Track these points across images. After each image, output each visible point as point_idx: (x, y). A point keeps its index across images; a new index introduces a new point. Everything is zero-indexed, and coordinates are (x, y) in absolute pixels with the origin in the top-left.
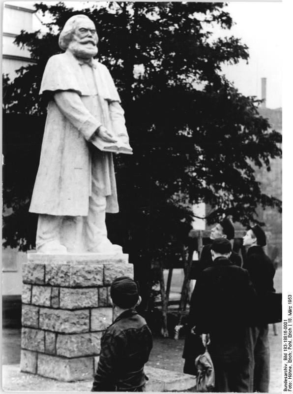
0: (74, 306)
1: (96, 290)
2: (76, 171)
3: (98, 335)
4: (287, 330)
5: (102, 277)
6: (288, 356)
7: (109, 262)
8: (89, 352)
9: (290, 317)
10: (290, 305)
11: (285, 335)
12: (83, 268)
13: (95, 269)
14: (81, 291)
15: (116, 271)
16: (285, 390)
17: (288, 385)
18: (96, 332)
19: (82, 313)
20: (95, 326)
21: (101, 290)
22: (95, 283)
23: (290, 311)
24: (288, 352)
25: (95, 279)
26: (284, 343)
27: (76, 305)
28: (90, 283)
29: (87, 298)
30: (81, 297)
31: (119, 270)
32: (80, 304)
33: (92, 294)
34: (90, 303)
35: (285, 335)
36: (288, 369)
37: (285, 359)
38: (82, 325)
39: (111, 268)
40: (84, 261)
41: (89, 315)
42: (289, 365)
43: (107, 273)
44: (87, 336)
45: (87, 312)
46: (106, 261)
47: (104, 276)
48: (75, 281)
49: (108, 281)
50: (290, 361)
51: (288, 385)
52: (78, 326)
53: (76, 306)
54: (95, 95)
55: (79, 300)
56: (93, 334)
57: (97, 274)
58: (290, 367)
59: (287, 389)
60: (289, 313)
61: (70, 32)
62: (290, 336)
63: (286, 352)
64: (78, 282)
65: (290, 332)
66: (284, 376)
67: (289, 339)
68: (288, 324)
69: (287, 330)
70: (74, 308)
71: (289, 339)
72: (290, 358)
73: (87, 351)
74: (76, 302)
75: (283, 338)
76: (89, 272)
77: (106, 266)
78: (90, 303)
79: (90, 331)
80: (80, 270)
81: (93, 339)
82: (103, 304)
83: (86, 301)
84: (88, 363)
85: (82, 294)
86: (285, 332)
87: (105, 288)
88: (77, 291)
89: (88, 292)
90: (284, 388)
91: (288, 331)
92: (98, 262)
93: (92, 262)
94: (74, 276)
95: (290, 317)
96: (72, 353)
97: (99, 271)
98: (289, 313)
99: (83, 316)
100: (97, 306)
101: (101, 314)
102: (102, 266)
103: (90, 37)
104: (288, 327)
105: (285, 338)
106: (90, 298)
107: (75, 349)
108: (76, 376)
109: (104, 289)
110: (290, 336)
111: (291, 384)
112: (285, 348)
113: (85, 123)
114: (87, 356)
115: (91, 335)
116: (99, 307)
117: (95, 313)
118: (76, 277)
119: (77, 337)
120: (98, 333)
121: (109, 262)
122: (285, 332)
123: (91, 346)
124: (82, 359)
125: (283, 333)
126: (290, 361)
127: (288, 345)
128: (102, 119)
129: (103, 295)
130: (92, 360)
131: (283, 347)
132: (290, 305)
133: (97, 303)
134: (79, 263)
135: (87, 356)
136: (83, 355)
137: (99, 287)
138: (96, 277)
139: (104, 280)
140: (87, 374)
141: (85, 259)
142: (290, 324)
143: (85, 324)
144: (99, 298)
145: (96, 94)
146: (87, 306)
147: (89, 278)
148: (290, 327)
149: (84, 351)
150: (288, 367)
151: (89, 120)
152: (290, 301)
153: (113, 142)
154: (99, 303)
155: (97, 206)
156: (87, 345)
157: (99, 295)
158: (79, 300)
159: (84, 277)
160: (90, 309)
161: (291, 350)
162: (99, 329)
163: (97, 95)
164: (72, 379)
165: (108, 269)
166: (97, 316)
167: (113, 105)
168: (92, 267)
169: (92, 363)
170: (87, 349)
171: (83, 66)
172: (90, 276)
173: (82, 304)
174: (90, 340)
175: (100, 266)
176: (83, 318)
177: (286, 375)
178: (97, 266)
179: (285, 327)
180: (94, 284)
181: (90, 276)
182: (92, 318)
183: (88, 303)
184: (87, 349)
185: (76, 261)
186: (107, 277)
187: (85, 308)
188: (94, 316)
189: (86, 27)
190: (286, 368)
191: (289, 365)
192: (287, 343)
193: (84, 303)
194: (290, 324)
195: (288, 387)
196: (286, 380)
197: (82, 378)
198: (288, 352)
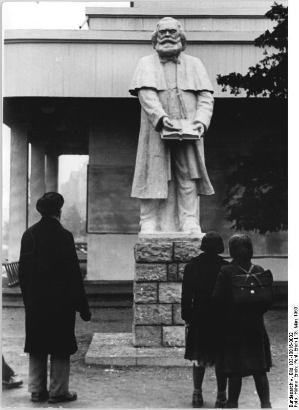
0: (140, 279)
1: (164, 266)
2: (155, 158)
3: (166, 307)
4: (293, 343)
5: (171, 254)
6: (294, 371)
7: (182, 240)
8: (156, 322)
9: (295, 330)
10: (296, 317)
11: (291, 349)
12: (149, 245)
13: (163, 246)
14: (147, 265)
15: (188, 249)
16: (291, 406)
17: (294, 400)
18: (165, 304)
19: (149, 285)
20: (163, 297)
21: (170, 266)
22: (162, 259)
23: (296, 324)
24: (294, 366)
25: (162, 256)
26: (289, 357)
27: (142, 278)
28: (156, 259)
29: (154, 272)
30: (147, 271)
31: (191, 248)
32: (146, 278)
33: (160, 269)
34: (157, 276)
35: (291, 349)
36: (294, 384)
37: (291, 374)
38: (148, 296)
39: (182, 246)
40: (154, 239)
41: (156, 287)
42: (295, 380)
43: (176, 251)
44: (154, 307)
45: (154, 285)
46: (175, 239)
47: (173, 252)
48: (140, 257)
49: (177, 258)
50: (296, 376)
51: (294, 400)
52: (144, 297)
53: (142, 279)
54: (174, 89)
55: (145, 273)
56: (160, 306)
57: (165, 251)
58: (296, 382)
59: (293, 405)
60: (295, 326)
61: (154, 35)
62: (296, 350)
63: (291, 367)
64: (144, 257)
65: (296, 346)
66: (289, 392)
67: (295, 353)
68: (294, 337)
69: (293, 343)
70: (140, 281)
71: (295, 353)
72: (296, 372)
73: (154, 321)
74: (143, 276)
75: (289, 352)
76: (156, 249)
77: (176, 244)
78: (157, 276)
79: (158, 302)
80: (146, 247)
81: (160, 310)
82: (171, 278)
83: (153, 275)
84: (155, 332)
85: (149, 268)
86: (290, 345)
87: (176, 265)
88: (143, 266)
89: (156, 267)
90: (289, 403)
91: (294, 345)
92: (169, 240)
93: (162, 240)
94: (139, 252)
95: (295, 330)
96: (138, 321)
97: (167, 249)
98: (295, 326)
99: (150, 288)
100: (166, 280)
101: (168, 288)
102: (171, 244)
103: (168, 37)
104: (294, 340)
105: (291, 352)
106: (158, 273)
107: (141, 317)
108: (141, 342)
109: (174, 266)
110: (296, 350)
111: (296, 399)
112: (290, 362)
113: (152, 115)
114: (154, 325)
115: (158, 307)
116: (168, 281)
117: (162, 286)
118: (141, 253)
119: (143, 307)
120: (167, 305)
121: (182, 240)
122: (290, 345)
123: (159, 317)
124: (149, 327)
125: (289, 347)
126: (296, 376)
127: (294, 359)
128: (181, 110)
129: (172, 271)
130: (160, 329)
131: (289, 361)
132: (296, 317)
133: (166, 278)
134: (148, 240)
135: (154, 325)
136: (151, 323)
137: (167, 263)
138: (163, 253)
139: (173, 257)
140: (153, 341)
141: (155, 237)
142: (296, 337)
143: (152, 295)
144: (168, 273)
145: (175, 87)
146: (154, 279)
147: (155, 254)
148: (296, 340)
149: (150, 320)
150: (294, 382)
151: (155, 113)
152: (296, 313)
153: (177, 130)
154: (167, 278)
155: (184, 189)
156: (154, 315)
157: (168, 270)
158: (145, 273)
159: (149, 253)
160: (158, 282)
161: (298, 364)
162: (168, 302)
163: (177, 88)
164: (138, 344)
165: (179, 247)
166: (165, 289)
167: (200, 95)
168: (159, 245)
169: (160, 332)
170: (154, 318)
171: (166, 64)
172: (156, 253)
173: (149, 278)
174: (157, 311)
175: (169, 244)
176: (149, 290)
177: (292, 390)
178: (164, 243)
179: (291, 340)
180: (160, 260)
181: (156, 253)
182: (159, 291)
183: (155, 277)
184: (154, 318)
185: (145, 239)
186: (177, 254)
187: (152, 281)
188: (162, 289)
189: (164, 29)
190: (292, 383)
191: (295, 380)
192: (293, 357)
193: (150, 277)
194: (296, 337)
195: (294, 403)
196: (291, 396)
197: (147, 345)
198: (294, 366)
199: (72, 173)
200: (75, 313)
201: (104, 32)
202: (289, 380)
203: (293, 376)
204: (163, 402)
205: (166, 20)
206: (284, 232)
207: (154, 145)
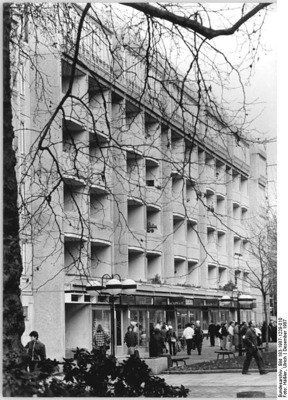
63: (280, 358)
177: (281, 380)
196: (281, 386)
203: (283, 366)
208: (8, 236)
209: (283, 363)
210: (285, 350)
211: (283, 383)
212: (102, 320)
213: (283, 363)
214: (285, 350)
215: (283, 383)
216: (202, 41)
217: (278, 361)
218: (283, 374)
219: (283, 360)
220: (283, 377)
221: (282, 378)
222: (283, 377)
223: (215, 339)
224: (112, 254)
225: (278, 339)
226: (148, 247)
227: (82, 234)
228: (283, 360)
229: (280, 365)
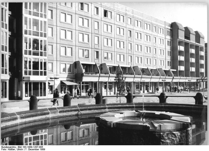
17: (5, 148)
42: (16, 149)
51: (5, 148)
63: (22, 147)
111: (6, 150)
131: (25, 146)
142: (25, 149)
148: (23, 150)
177: (10, 147)
190: (14, 147)
195: (4, 148)
196: (7, 147)
199: (137, 66)
200: (14, 79)
201: (112, 51)
202: (15, 146)
203: (18, 148)
204: (117, 101)
205: (104, 80)
206: (97, 142)
207: (181, 87)
208: (161, 144)
209: (19, 148)
210: (29, 149)
211: (9, 148)
212: (39, 75)
213: (19, 148)
214: (29, 149)
215: (9, 148)
216: (57, 60)
217: (21, 146)
218: (13, 148)
219: (21, 148)
220: (12, 148)
221: (11, 148)
222: (12, 148)
223: (19, 91)
224: (98, 115)
225: (38, 146)
226: (75, 47)
227: (75, 141)
228: (21, 148)
229: (18, 147)
